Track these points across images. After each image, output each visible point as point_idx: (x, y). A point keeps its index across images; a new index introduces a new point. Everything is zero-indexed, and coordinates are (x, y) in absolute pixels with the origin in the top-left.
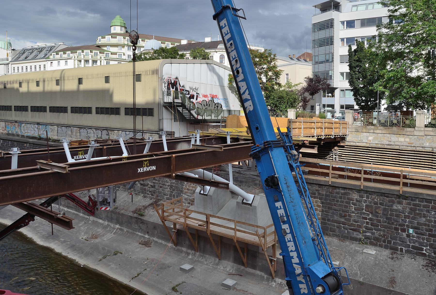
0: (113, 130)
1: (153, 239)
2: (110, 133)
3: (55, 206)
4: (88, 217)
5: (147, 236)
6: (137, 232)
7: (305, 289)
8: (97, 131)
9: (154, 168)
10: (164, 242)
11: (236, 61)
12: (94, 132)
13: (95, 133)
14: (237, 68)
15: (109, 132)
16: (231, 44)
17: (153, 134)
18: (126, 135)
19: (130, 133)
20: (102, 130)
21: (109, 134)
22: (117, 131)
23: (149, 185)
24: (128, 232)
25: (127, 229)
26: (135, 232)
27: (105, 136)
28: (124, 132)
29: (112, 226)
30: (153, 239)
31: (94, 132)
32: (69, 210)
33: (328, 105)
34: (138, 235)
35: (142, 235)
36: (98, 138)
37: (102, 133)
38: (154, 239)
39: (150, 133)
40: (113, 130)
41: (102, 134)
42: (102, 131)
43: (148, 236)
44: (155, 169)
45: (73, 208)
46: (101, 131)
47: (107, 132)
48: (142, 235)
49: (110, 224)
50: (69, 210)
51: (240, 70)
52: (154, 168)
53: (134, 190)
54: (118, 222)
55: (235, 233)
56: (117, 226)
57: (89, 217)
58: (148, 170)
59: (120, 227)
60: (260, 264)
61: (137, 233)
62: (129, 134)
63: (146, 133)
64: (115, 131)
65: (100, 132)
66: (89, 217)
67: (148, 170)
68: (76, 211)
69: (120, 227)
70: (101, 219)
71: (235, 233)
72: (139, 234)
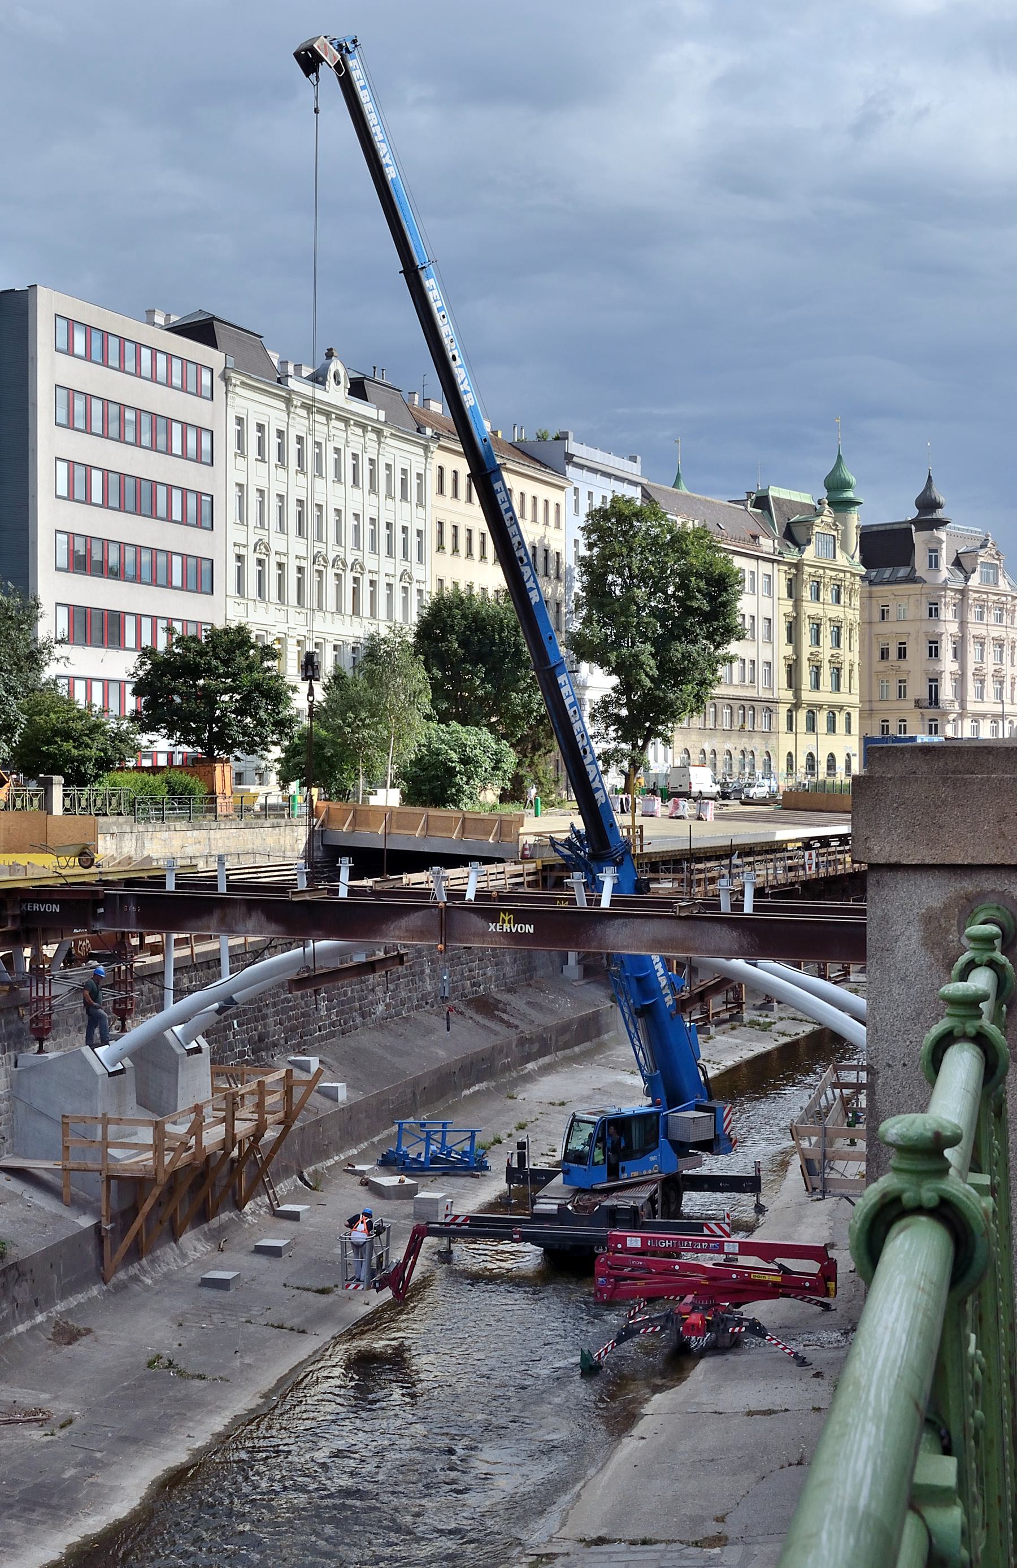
1: (57, 1313)
5: (40, 1318)
6: (10, 1330)
7: (611, 1007)
9: (530, 929)
10: (80, 1296)
11: (582, 736)
14: (583, 747)
16: (575, 712)
30: (57, 1313)
33: (612, 1178)
35: (28, 1324)
38: (58, 1308)
43: (41, 1312)
44: (532, 931)
48: (28, 1324)
51: (587, 748)
52: (530, 929)
55: (314, 393)
58: (514, 931)
60: (634, 1242)
67: (514, 931)
71: (314, 393)
72: (21, 1328)
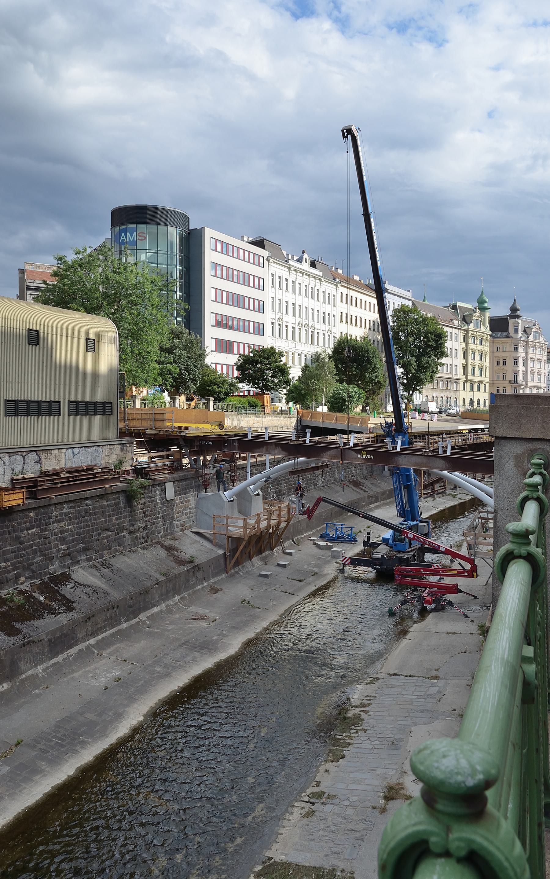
0: (47, 450)
2: (42, 456)
3: (66, 656)
4: (137, 620)
5: (205, 584)
6: (195, 588)
8: (13, 458)
9: (372, 457)
12: (4, 463)
13: (7, 464)
15: (40, 455)
17: (113, 446)
18: (74, 455)
19: (81, 449)
20: (24, 454)
21: (40, 460)
22: (57, 451)
23: (141, 529)
24: (189, 595)
25: (187, 593)
26: (195, 589)
27: (33, 464)
28: (70, 450)
29: (172, 603)
31: (4, 463)
32: (100, 637)
34: (199, 589)
36: (16, 475)
37: (24, 461)
38: (211, 581)
39: (110, 445)
40: (47, 450)
41: (24, 463)
42: (24, 457)
45: (104, 627)
46: (22, 455)
47: (37, 457)
48: (201, 586)
49: (168, 602)
50: (100, 637)
52: (372, 457)
53: (124, 547)
54: (176, 591)
56: (177, 598)
57: (139, 618)
59: (179, 597)
61: (197, 588)
62: (79, 453)
63: (104, 447)
64: (52, 451)
65: (19, 458)
66: (139, 618)
68: (113, 627)
69: (179, 597)
70: (154, 606)
72: (199, 587)
